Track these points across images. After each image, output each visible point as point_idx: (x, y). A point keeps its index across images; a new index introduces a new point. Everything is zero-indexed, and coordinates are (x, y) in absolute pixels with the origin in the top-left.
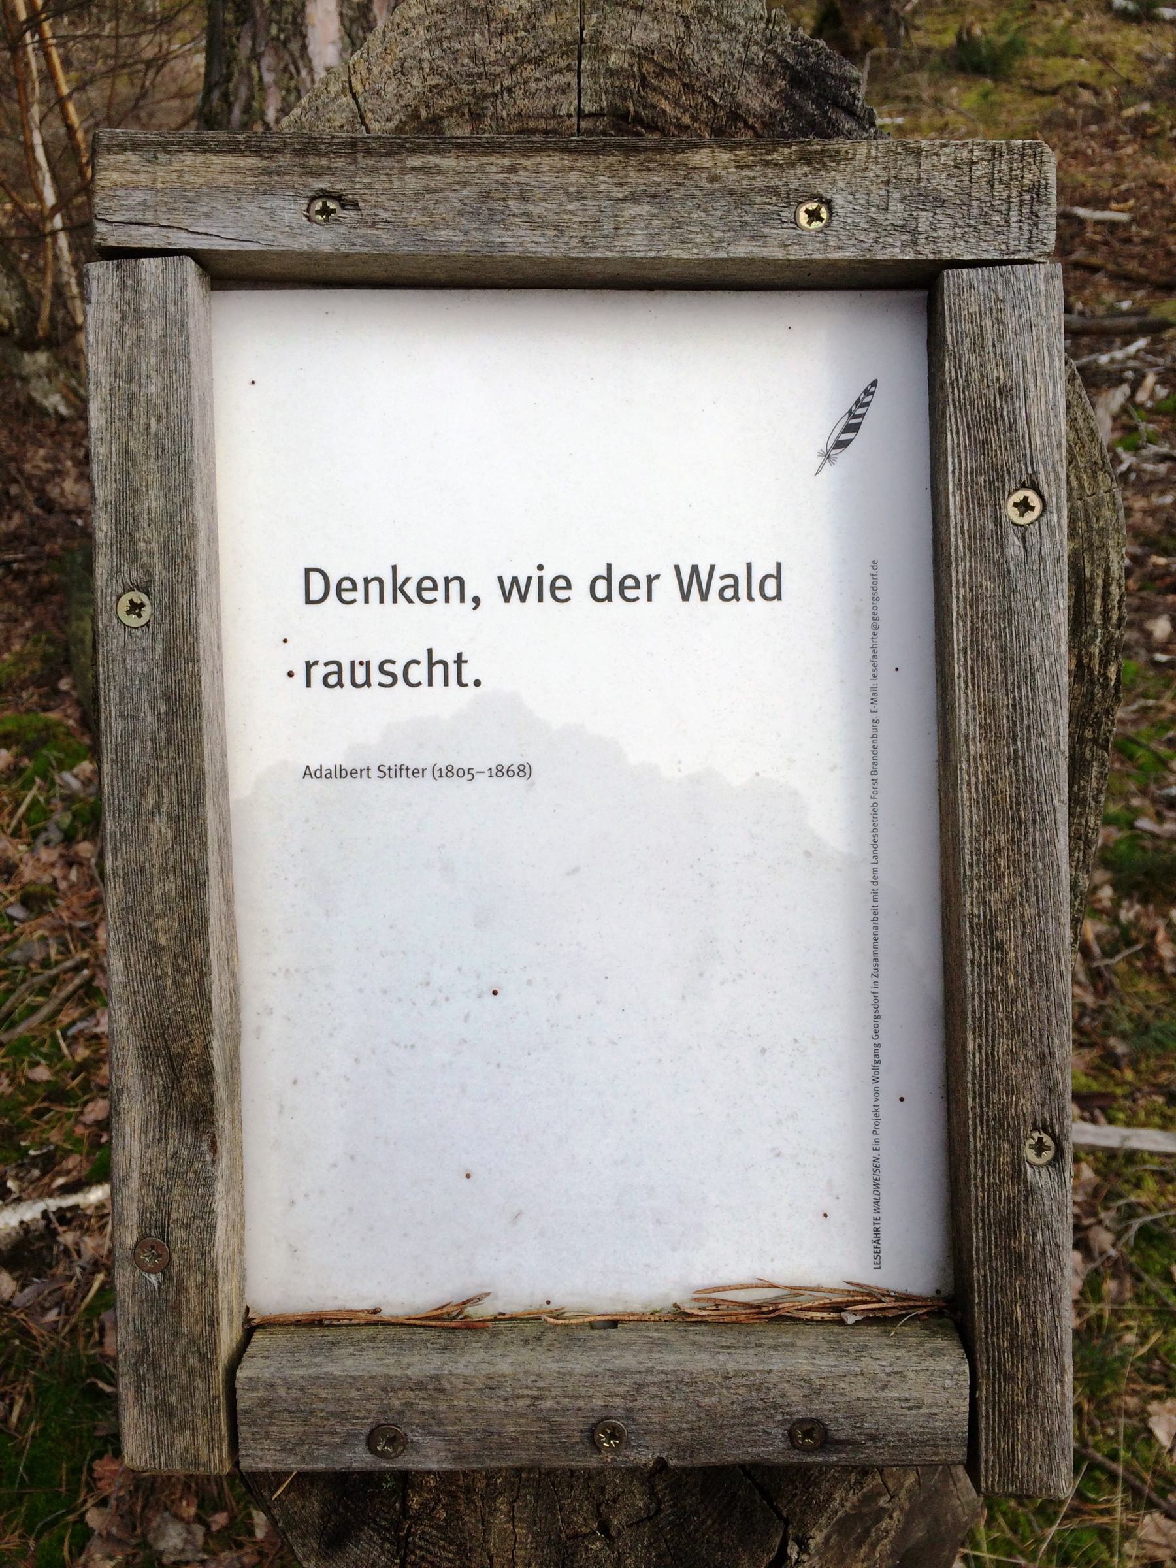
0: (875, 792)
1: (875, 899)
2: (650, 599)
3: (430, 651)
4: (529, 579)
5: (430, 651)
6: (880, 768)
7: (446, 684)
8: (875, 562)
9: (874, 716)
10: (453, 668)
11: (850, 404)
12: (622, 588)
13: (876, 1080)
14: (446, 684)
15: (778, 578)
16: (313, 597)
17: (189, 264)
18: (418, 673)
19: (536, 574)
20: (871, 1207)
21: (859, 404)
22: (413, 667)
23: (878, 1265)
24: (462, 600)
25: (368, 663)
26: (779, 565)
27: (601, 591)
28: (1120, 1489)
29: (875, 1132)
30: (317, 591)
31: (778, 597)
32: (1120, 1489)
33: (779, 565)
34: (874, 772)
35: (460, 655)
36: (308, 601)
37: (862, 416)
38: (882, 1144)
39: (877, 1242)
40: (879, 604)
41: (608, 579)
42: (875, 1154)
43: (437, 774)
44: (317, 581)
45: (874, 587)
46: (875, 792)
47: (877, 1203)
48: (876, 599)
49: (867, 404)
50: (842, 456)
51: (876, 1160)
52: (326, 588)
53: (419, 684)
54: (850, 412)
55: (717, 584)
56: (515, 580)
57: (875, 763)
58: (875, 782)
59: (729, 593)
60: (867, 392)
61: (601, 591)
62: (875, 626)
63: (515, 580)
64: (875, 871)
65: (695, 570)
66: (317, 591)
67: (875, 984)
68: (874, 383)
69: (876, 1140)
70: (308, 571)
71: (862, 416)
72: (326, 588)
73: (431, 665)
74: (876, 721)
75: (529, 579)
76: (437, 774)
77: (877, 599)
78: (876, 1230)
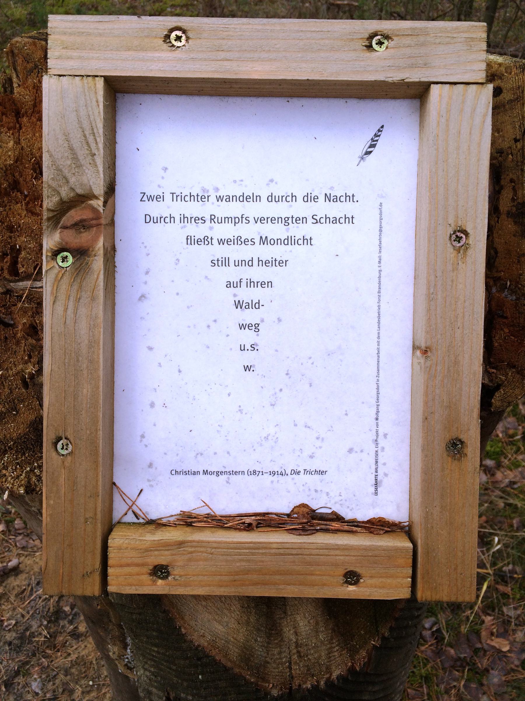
0: (379, 300)
1: (378, 345)
2: (350, 198)
8: (381, 203)
9: (379, 268)
10: (309, 241)
11: (372, 135)
12: (246, 199)
15: (252, 261)
17: (103, 78)
21: (376, 135)
27: (306, 200)
28: (11, 31)
30: (148, 220)
31: (252, 266)
32: (11, 31)
34: (379, 292)
36: (146, 222)
37: (377, 141)
40: (382, 221)
42: (376, 449)
44: (148, 217)
46: (379, 300)
49: (379, 136)
50: (369, 158)
54: (372, 139)
55: (244, 305)
57: (380, 288)
58: (379, 296)
60: (379, 131)
61: (306, 200)
62: (381, 231)
64: (379, 333)
65: (151, 196)
66: (148, 220)
67: (378, 380)
68: (382, 127)
70: (146, 215)
71: (377, 141)
73: (171, 218)
76: (249, 473)
77: (382, 219)
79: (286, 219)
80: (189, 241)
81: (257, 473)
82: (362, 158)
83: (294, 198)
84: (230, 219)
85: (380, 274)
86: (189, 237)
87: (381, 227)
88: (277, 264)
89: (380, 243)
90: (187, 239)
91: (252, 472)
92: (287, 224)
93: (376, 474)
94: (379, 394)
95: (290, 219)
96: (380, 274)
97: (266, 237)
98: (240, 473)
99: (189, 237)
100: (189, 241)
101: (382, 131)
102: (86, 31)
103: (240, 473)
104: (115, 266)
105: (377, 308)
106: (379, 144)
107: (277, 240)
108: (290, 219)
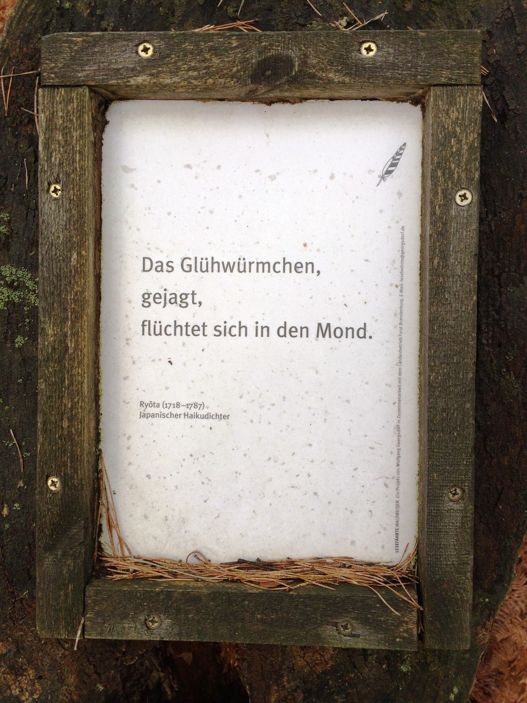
1: (400, 382)
3: (240, 322)
4: (234, 263)
5: (240, 322)
6: (403, 360)
7: (181, 335)
11: (393, 153)
12: (290, 332)
13: (398, 465)
14: (181, 335)
15: (365, 329)
16: (146, 269)
18: (170, 330)
19: (237, 261)
20: (394, 523)
21: (398, 154)
22: (168, 328)
23: (397, 550)
24: (313, 272)
25: (149, 321)
26: (365, 324)
29: (397, 489)
30: (148, 267)
33: (365, 324)
35: (187, 323)
37: (399, 159)
38: (400, 495)
39: (397, 540)
41: (285, 328)
42: (397, 499)
43: (165, 406)
44: (148, 262)
45: (403, 238)
47: (397, 522)
48: (403, 244)
49: (401, 154)
50: (389, 178)
51: (397, 502)
52: (151, 266)
53: (171, 334)
54: (393, 157)
56: (229, 263)
59: (173, 301)
60: (401, 149)
63: (229, 263)
66: (148, 267)
68: (405, 145)
69: (398, 493)
70: (144, 259)
71: (399, 159)
72: (151, 266)
74: (397, 502)
75: (234, 263)
76: (165, 406)
77: (404, 244)
78: (397, 534)
79: (184, 297)
80: (146, 328)
81: (199, 406)
82: (383, 178)
83: (243, 330)
84: (266, 266)
85: (402, 304)
86: (146, 323)
87: (403, 252)
88: (190, 332)
89: (402, 270)
90: (143, 325)
91: (176, 405)
92: (146, 304)
93: (397, 528)
94: (400, 436)
95: (190, 297)
96: (402, 304)
97: (328, 325)
98: (254, 266)
99: (146, 323)
100: (146, 328)
101: (404, 149)
102: (289, 32)
103: (254, 266)
104: (102, 144)
105: (399, 341)
106: (401, 163)
107: (347, 329)
108: (190, 297)
